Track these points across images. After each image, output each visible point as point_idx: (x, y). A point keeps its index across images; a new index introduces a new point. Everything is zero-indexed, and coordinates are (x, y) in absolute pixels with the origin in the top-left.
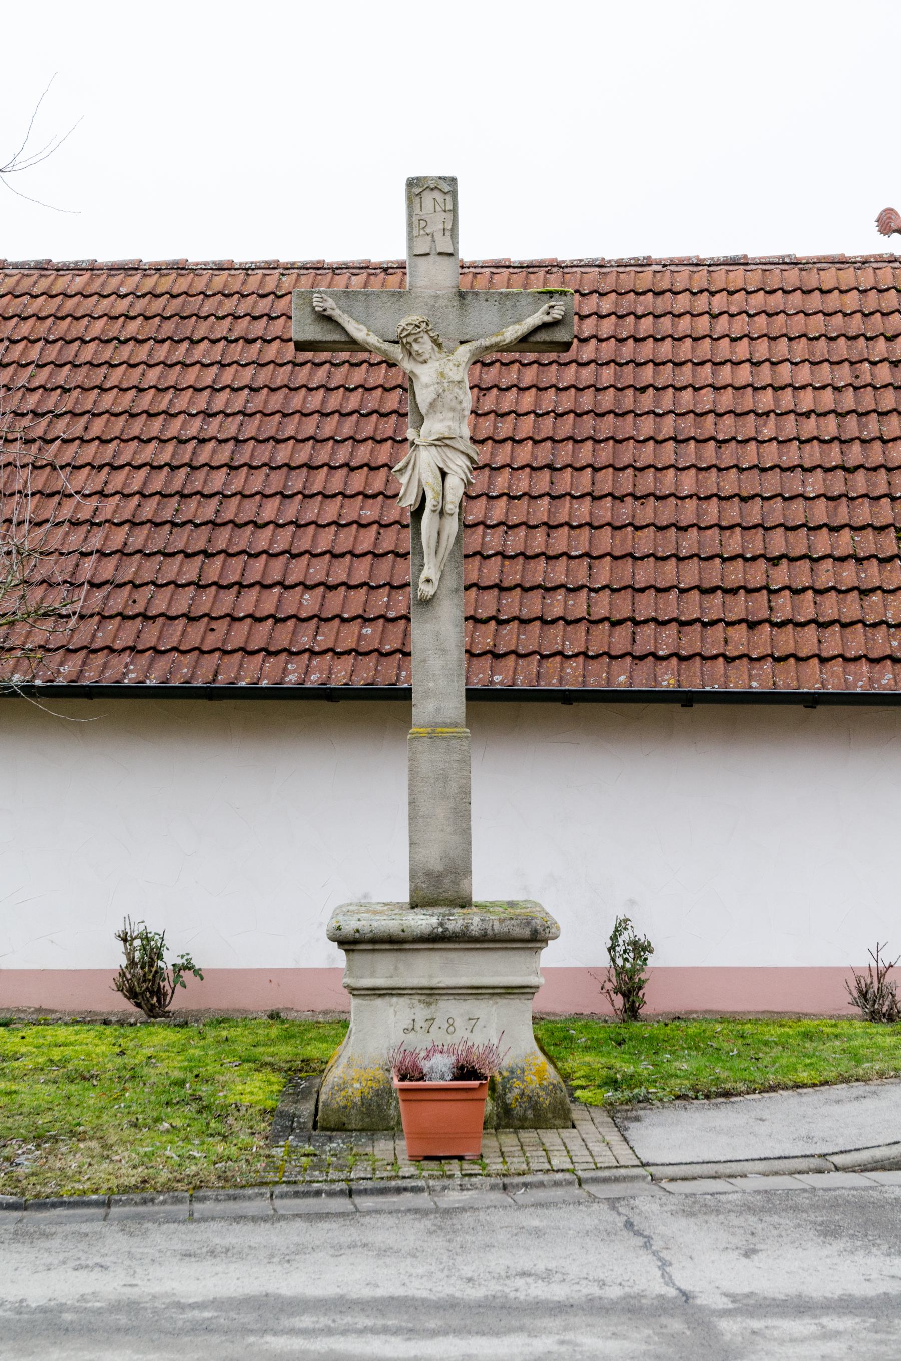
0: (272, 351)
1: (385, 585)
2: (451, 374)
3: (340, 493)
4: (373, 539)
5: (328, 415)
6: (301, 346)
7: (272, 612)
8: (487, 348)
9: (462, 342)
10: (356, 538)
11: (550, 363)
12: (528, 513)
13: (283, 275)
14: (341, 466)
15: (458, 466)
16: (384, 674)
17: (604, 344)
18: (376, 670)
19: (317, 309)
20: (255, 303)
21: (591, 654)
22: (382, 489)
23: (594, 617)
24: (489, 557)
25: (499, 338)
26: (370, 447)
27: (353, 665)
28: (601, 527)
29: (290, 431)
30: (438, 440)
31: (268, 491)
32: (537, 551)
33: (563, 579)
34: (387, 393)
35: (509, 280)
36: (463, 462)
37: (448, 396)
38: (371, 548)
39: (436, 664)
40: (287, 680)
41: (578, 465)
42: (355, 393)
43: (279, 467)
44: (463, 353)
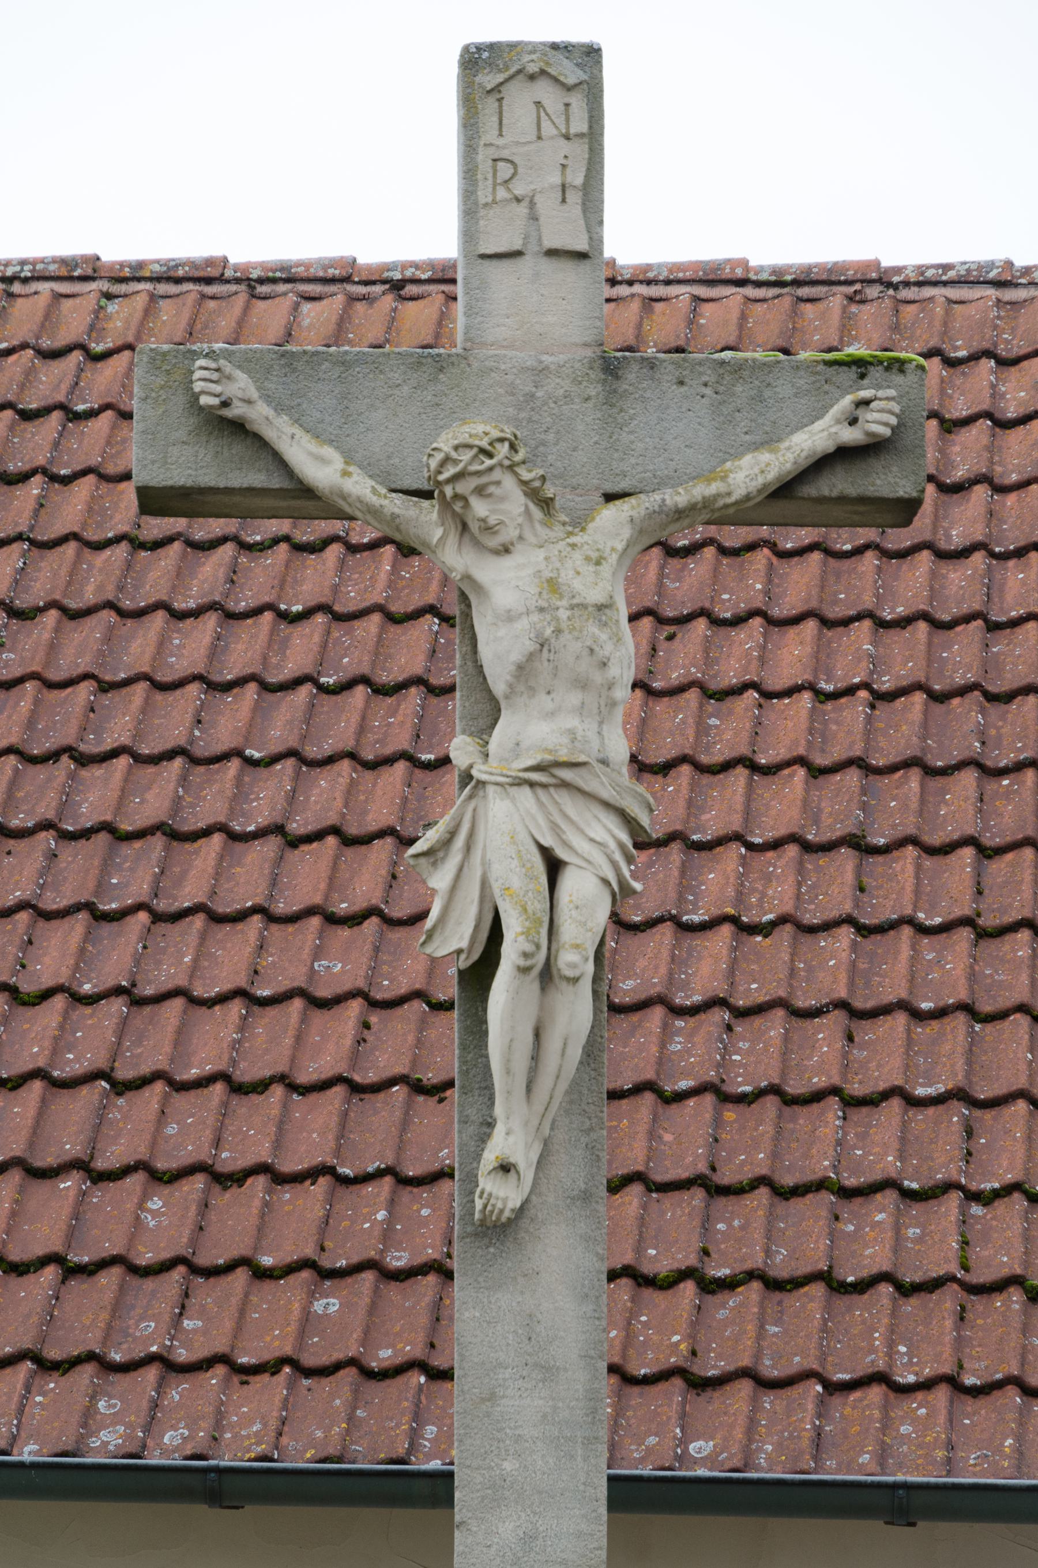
0: (72, 508)
1: (379, 1174)
2: (577, 584)
3: (256, 910)
4: (348, 1042)
5: (227, 687)
6: (154, 501)
7: (56, 1246)
8: (680, 514)
9: (610, 498)
10: (299, 1038)
11: (858, 551)
12: (793, 972)
13: (109, 296)
14: (260, 834)
15: (595, 845)
16: (366, 1430)
17: (1011, 499)
18: (351, 1418)
19: (204, 400)
20: (30, 373)
21: (970, 1380)
22: (376, 900)
23: (981, 1276)
24: (680, 1097)
25: (714, 488)
26: (343, 781)
27: (285, 1404)
28: (1001, 1015)
29: (118, 732)
30: (537, 768)
31: (52, 902)
32: (819, 1081)
33: (890, 1164)
34: (394, 629)
35: (743, 317)
36: (609, 832)
37: (570, 647)
38: (341, 1068)
39: (524, 1406)
40: (95, 1443)
41: (935, 839)
42: (305, 628)
43: (85, 834)
44: (613, 525)
